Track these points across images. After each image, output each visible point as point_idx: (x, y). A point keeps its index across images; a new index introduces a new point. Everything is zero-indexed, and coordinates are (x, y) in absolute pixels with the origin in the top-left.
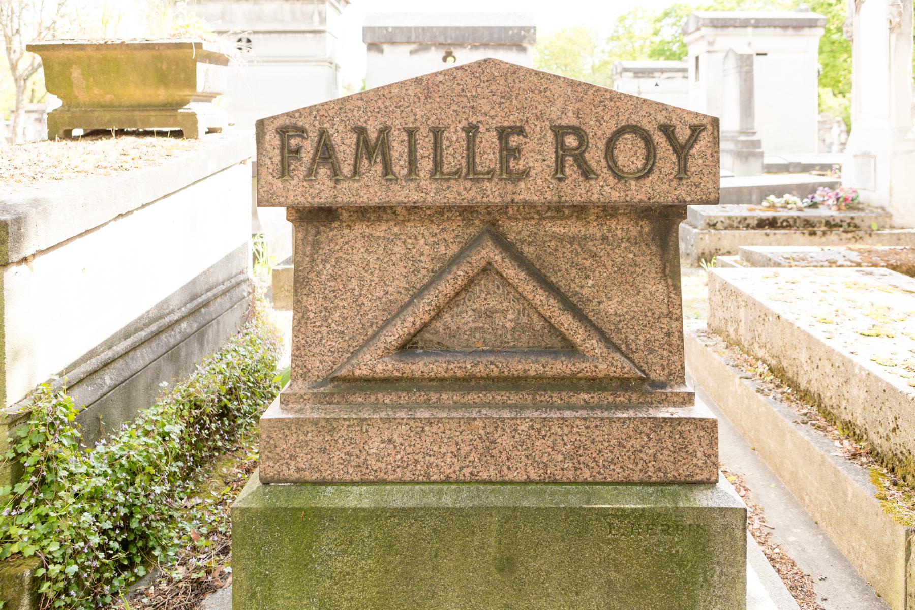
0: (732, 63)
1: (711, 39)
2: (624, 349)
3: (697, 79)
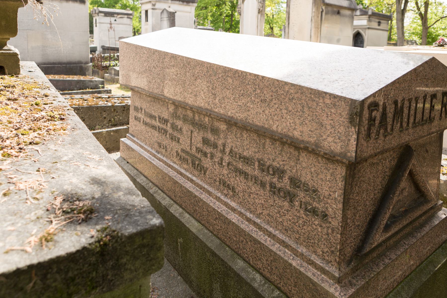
0: (165, 15)
1: (154, 3)
2: (251, 263)
3: (147, 20)
